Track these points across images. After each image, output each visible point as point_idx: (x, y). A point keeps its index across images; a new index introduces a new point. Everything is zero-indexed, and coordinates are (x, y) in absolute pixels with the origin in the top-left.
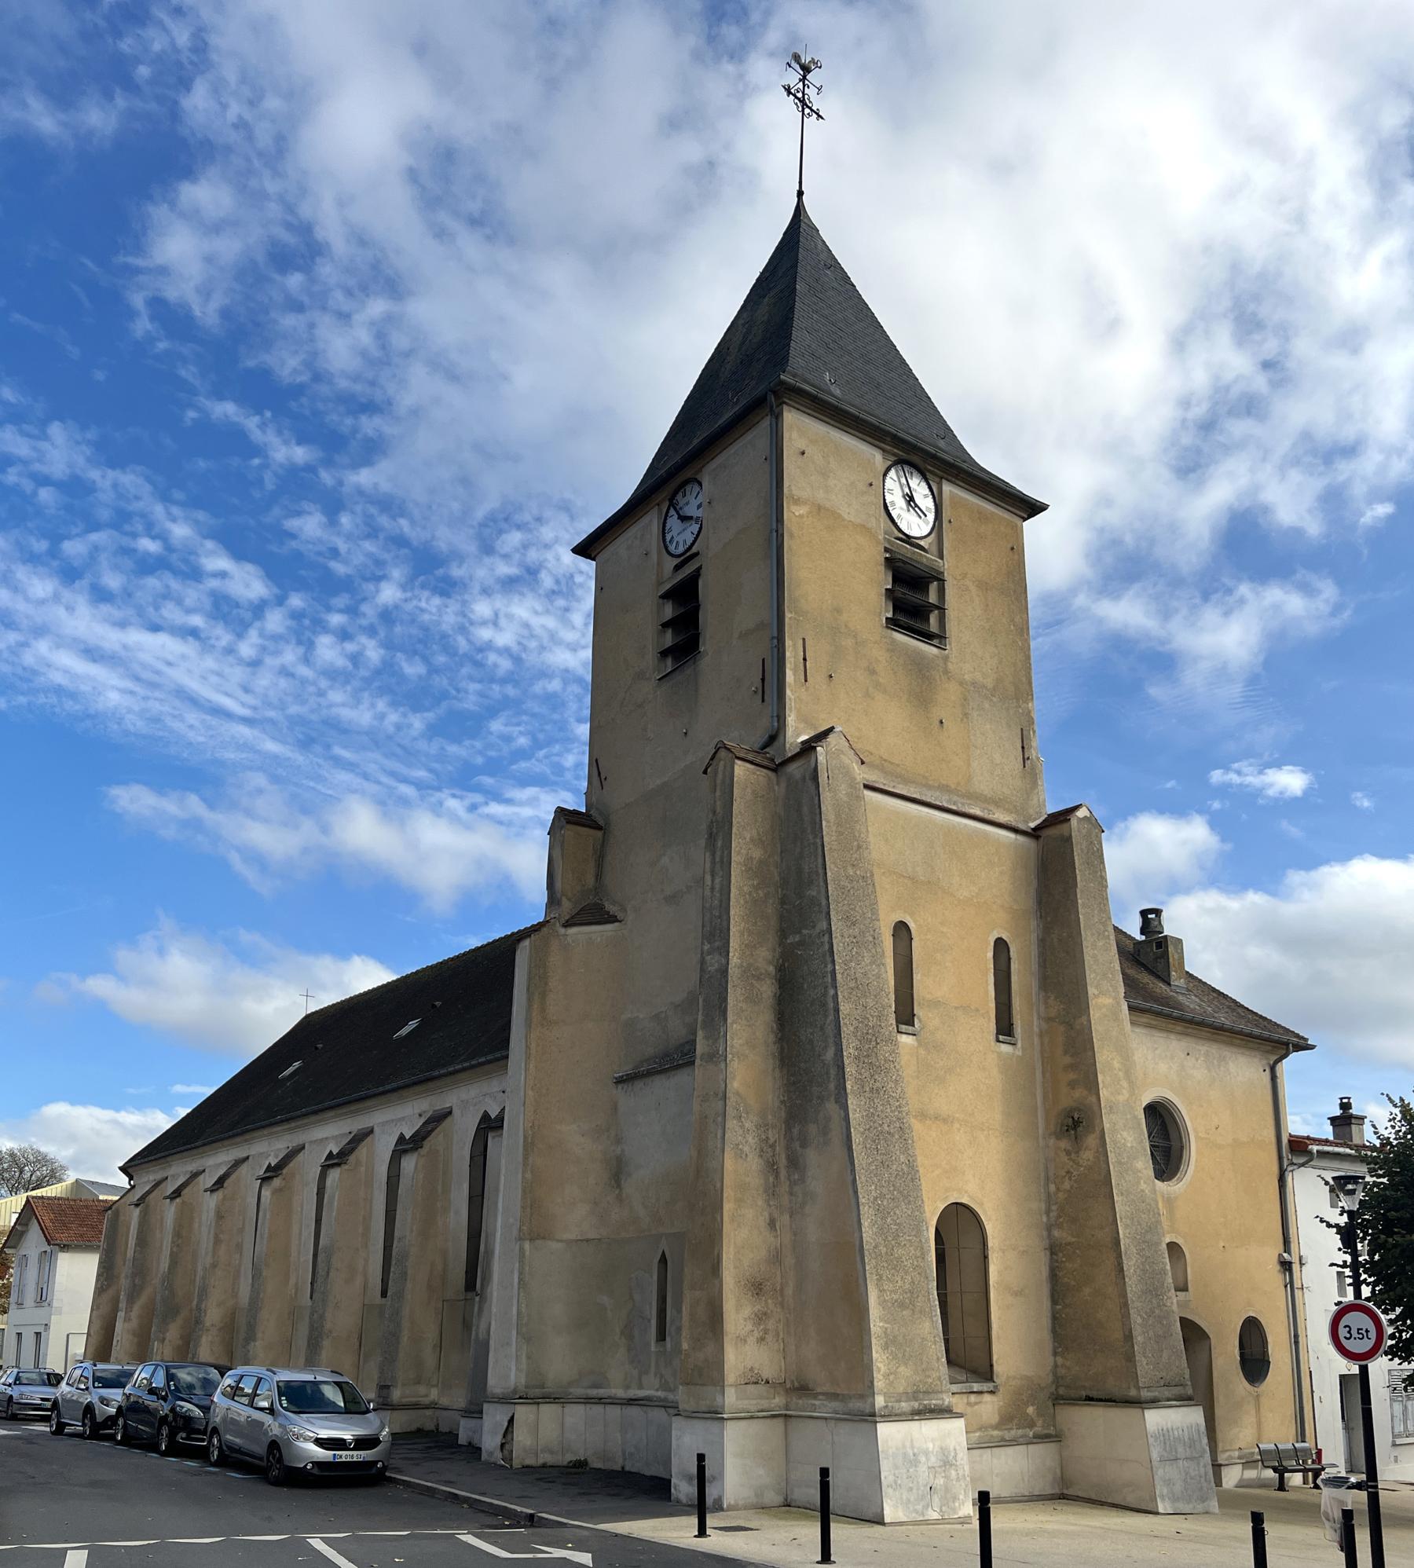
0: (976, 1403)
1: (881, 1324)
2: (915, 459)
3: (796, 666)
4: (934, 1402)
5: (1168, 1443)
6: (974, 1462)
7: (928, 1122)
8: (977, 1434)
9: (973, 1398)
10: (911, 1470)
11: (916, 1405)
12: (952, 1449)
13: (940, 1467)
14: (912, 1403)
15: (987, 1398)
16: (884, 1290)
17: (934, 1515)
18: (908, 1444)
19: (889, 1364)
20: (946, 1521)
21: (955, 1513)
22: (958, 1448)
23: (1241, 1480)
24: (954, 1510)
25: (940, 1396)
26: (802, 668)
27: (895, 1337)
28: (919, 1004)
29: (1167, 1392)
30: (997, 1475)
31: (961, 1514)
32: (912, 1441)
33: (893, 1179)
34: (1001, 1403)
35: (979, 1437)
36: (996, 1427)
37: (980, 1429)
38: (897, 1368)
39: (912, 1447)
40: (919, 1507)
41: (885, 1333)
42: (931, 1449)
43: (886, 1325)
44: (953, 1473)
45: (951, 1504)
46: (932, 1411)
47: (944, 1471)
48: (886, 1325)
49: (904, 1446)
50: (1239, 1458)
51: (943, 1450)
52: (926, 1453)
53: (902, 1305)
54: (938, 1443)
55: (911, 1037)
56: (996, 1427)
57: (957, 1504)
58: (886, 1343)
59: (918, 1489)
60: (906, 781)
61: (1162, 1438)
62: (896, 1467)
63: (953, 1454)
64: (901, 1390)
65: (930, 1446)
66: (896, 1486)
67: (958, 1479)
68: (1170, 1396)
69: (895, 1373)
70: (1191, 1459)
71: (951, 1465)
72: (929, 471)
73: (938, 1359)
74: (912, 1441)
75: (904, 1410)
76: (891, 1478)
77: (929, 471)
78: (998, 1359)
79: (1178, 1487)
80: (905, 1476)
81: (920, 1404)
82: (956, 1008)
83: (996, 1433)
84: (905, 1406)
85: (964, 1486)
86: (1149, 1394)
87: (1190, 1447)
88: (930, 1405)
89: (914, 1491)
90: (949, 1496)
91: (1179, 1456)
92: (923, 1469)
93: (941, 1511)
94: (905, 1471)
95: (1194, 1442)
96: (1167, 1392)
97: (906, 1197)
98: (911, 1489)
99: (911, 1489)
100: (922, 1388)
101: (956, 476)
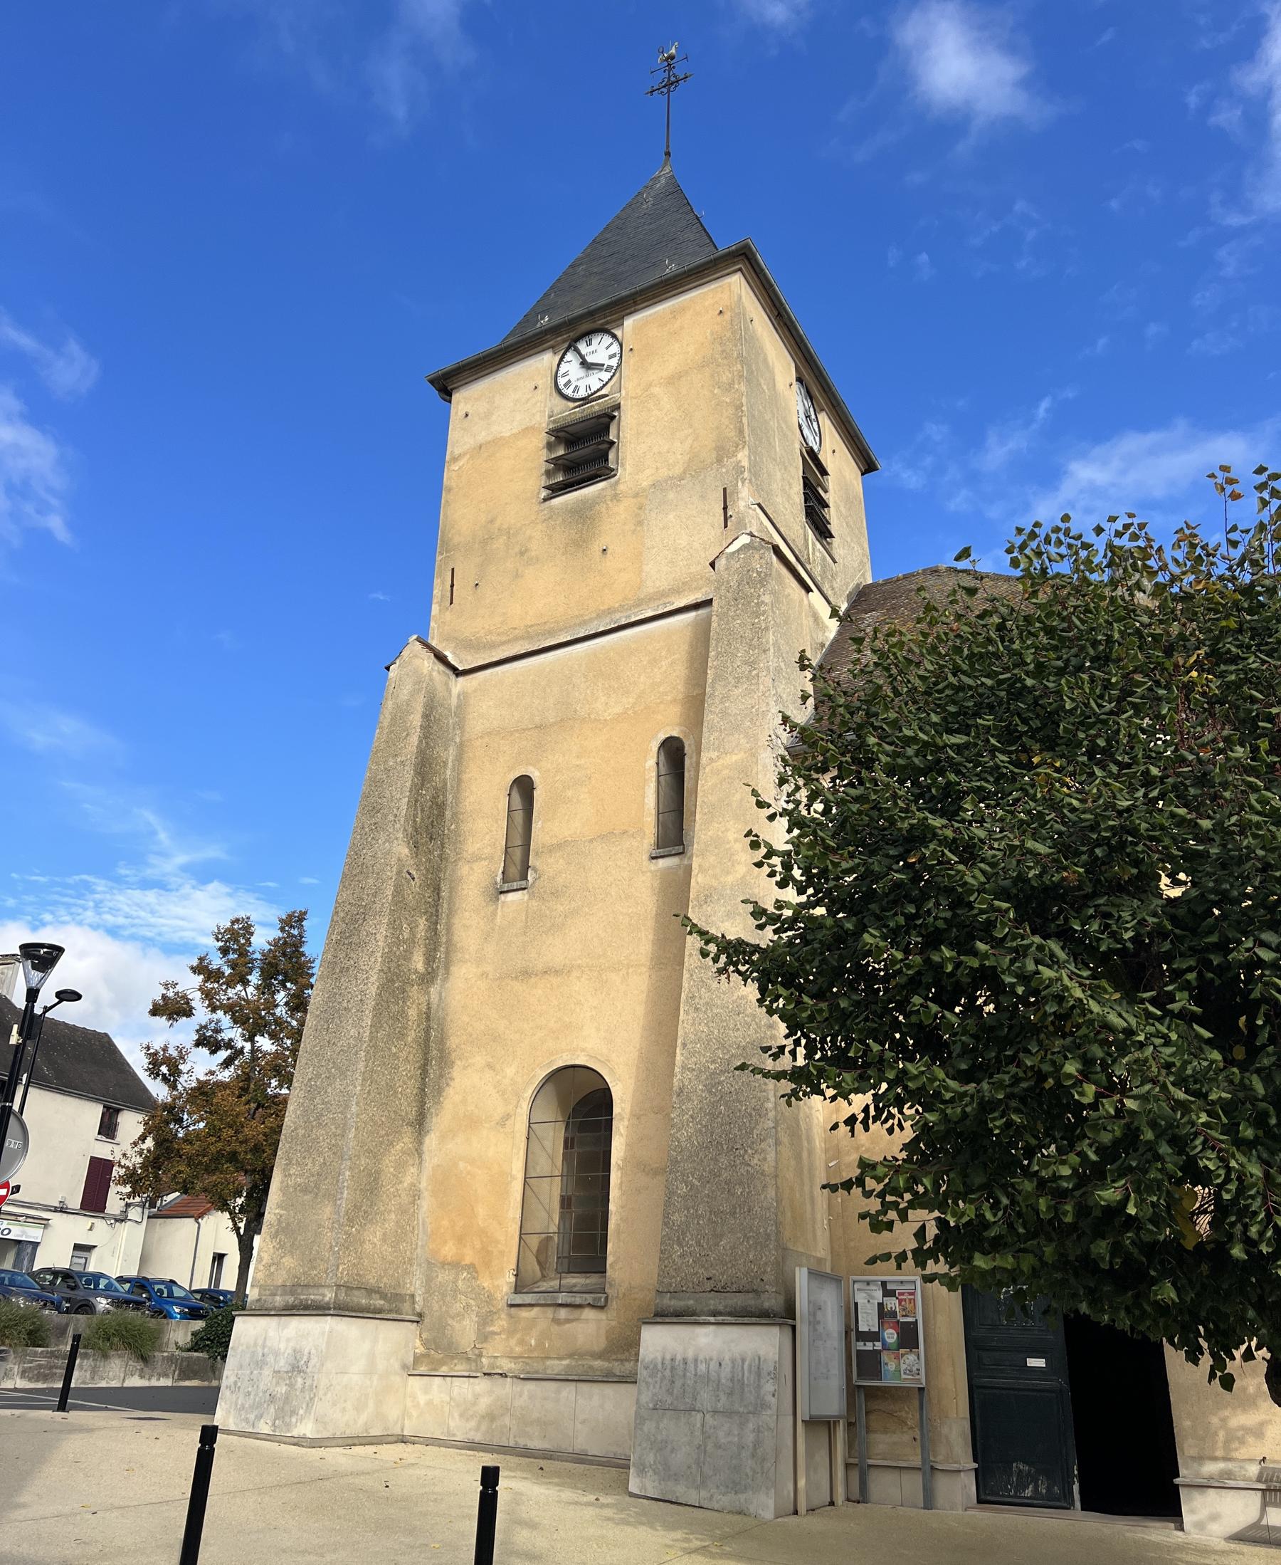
0: (568, 1321)
1: (277, 1211)
2: (585, 327)
3: (443, 596)
4: (312, 1297)
5: (678, 1383)
6: (545, 1399)
7: (533, 980)
8: (565, 1362)
9: (563, 1313)
10: (255, 1372)
11: (291, 1300)
12: (306, 1352)
13: (287, 1372)
14: (287, 1298)
15: (588, 1314)
16: (290, 1175)
17: (264, 1428)
18: (260, 1342)
19: (274, 1253)
20: (278, 1438)
21: (288, 1431)
22: (313, 1351)
23: (1256, 1526)
24: (288, 1426)
25: (321, 1290)
26: (449, 594)
27: (288, 1224)
28: (537, 854)
29: (714, 1302)
30: (583, 1422)
31: (295, 1433)
32: (265, 1338)
33: (334, 1056)
34: (613, 1323)
35: (568, 1365)
36: (600, 1356)
37: (571, 1356)
38: (282, 1258)
39: (264, 1346)
40: (252, 1417)
41: (279, 1220)
42: (282, 1350)
43: (282, 1212)
44: (300, 1380)
45: (287, 1419)
46: (306, 1307)
47: (290, 1378)
48: (282, 1212)
49: (256, 1344)
50: (1259, 1480)
51: (296, 1353)
52: (277, 1354)
53: (305, 1190)
54: (291, 1344)
55: (520, 892)
56: (600, 1356)
57: (294, 1420)
58: (277, 1232)
59: (256, 1395)
60: (551, 633)
61: (668, 1373)
62: (241, 1367)
63: (305, 1359)
64: (280, 1282)
65: (282, 1346)
66: (235, 1388)
67: (303, 1390)
68: (721, 1308)
69: (278, 1264)
70: (728, 1413)
71: (299, 1372)
72: (608, 323)
73: (331, 1247)
74: (265, 1338)
75: (277, 1304)
76: (232, 1379)
77: (602, 324)
78: (615, 1262)
79: (681, 1457)
80: (247, 1378)
81: (296, 1298)
82: (591, 841)
83: (598, 1363)
84: (279, 1300)
85: (308, 1398)
86: (673, 1302)
87: (731, 1394)
88: (307, 1300)
89: (252, 1397)
90: (287, 1408)
91: (698, 1406)
92: (267, 1372)
93: (274, 1424)
94: (248, 1372)
95: (741, 1382)
96: (714, 1302)
97: (342, 1073)
98: (249, 1393)
99: (249, 1393)
100: (303, 1281)
101: (635, 303)
